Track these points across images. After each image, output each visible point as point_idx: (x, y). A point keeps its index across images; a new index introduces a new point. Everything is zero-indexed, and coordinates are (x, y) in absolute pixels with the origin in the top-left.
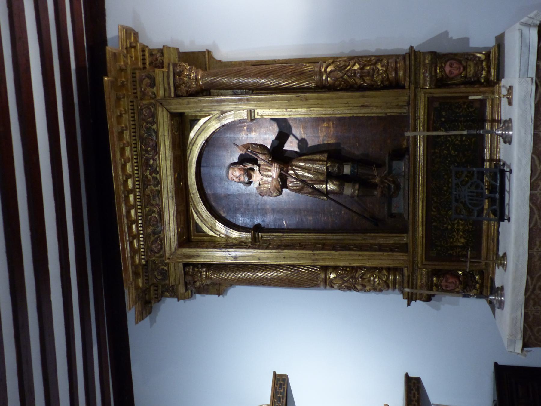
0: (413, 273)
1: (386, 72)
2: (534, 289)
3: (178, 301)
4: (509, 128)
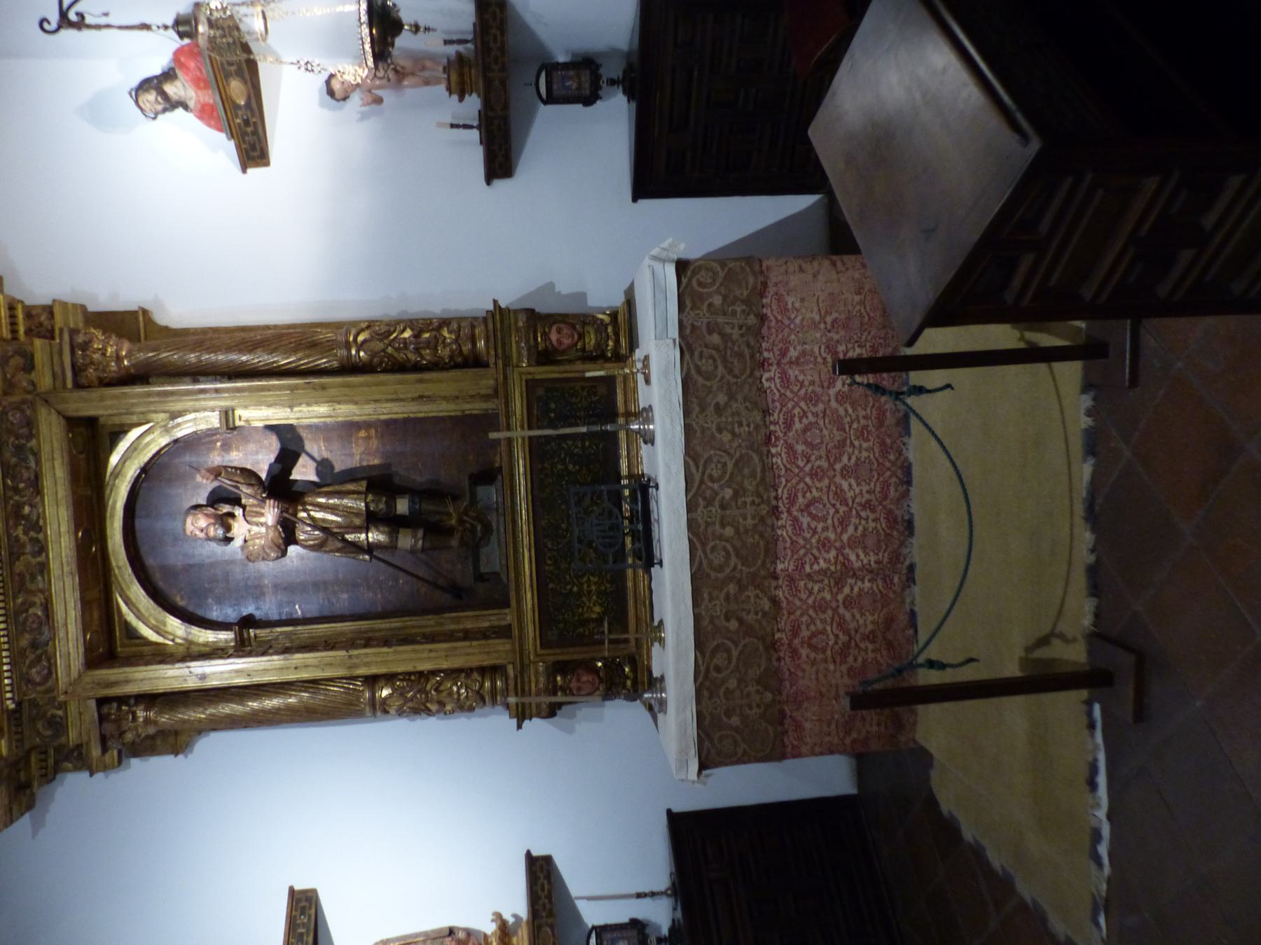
0: (522, 673)
1: (456, 341)
2: (708, 671)
3: (91, 775)
4: (649, 420)
